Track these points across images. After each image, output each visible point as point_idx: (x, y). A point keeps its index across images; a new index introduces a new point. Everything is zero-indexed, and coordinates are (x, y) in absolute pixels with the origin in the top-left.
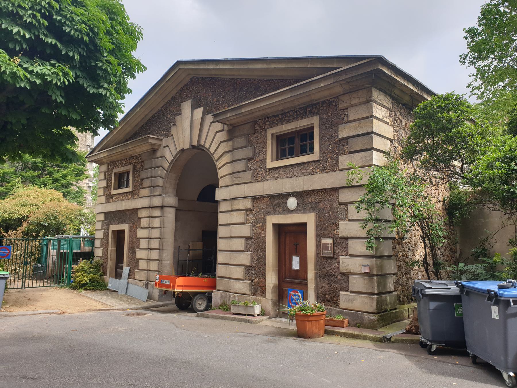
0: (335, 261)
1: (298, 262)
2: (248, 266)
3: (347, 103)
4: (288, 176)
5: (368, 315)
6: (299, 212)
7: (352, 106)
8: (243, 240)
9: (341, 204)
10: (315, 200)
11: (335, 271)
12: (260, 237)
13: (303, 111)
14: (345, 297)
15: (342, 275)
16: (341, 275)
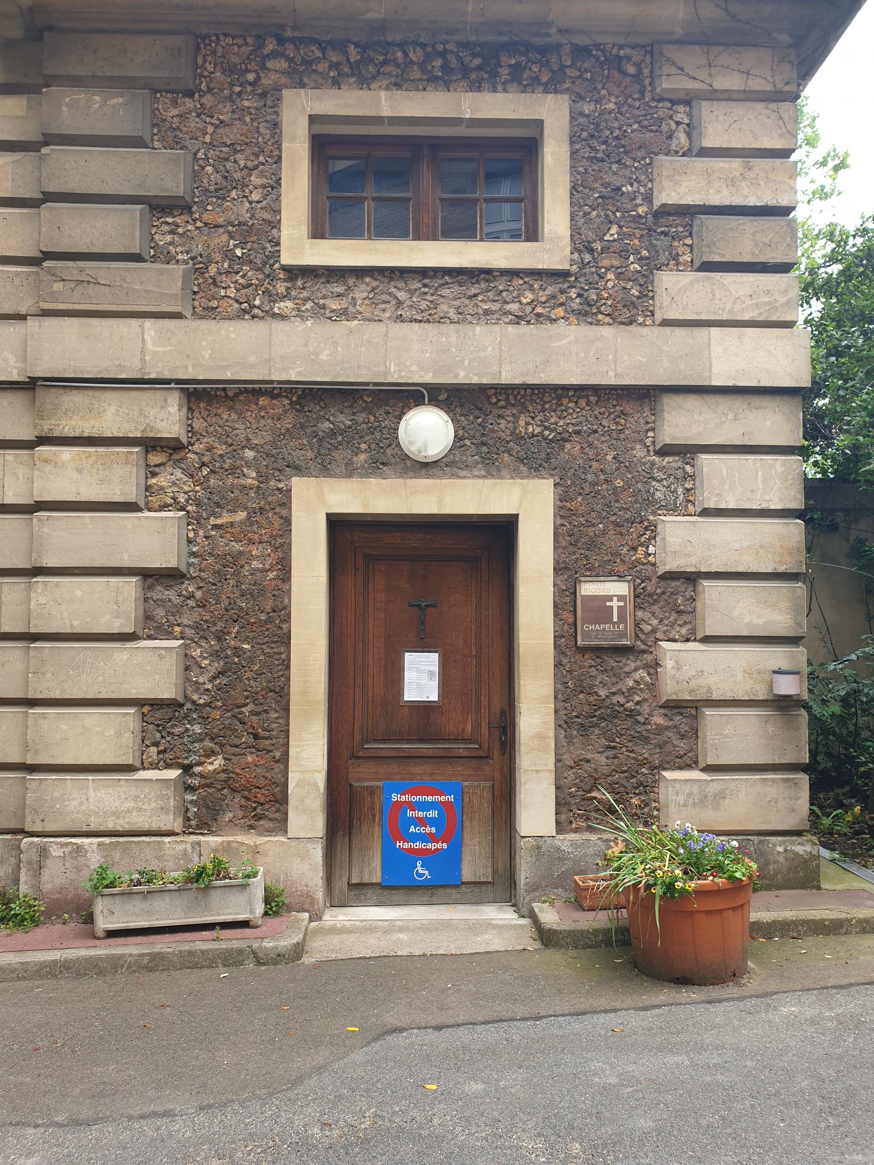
0: (639, 663)
1: (431, 673)
2: (156, 704)
3: (695, 78)
4: (407, 314)
5: (784, 842)
6: (463, 473)
7: (714, 95)
8: (130, 586)
9: (666, 451)
10: (546, 428)
11: (637, 698)
12: (237, 574)
13: (477, 61)
14: (687, 788)
15: (669, 713)
16: (662, 711)
